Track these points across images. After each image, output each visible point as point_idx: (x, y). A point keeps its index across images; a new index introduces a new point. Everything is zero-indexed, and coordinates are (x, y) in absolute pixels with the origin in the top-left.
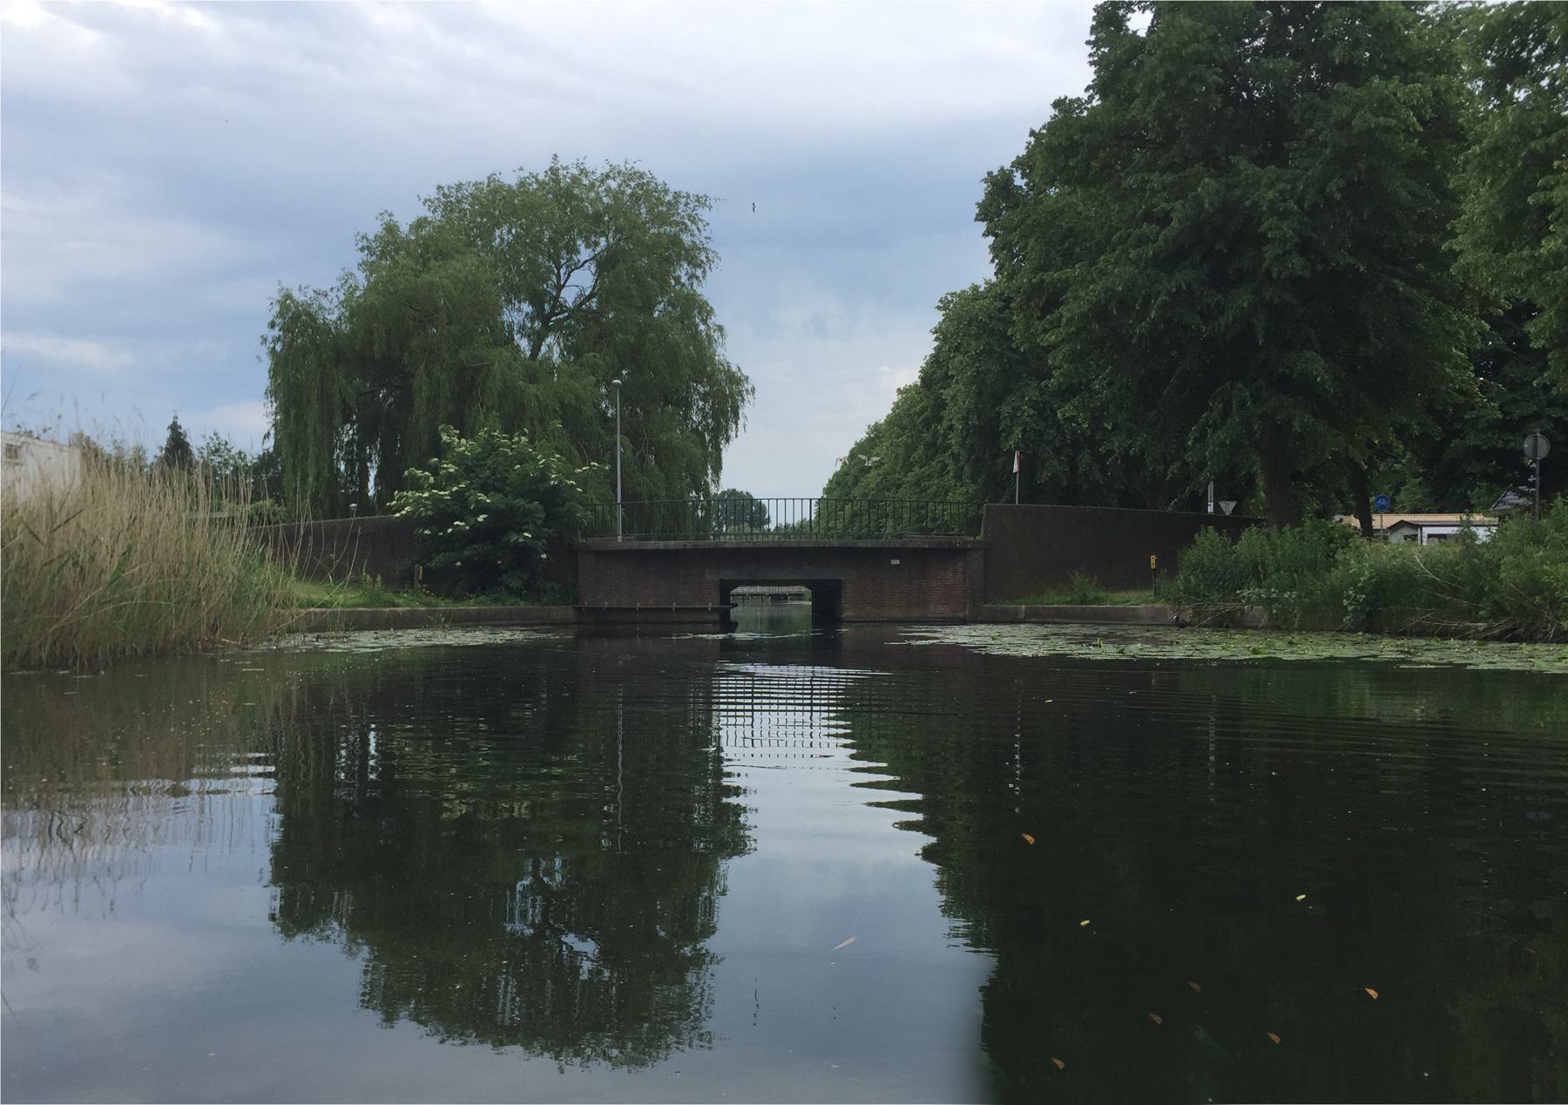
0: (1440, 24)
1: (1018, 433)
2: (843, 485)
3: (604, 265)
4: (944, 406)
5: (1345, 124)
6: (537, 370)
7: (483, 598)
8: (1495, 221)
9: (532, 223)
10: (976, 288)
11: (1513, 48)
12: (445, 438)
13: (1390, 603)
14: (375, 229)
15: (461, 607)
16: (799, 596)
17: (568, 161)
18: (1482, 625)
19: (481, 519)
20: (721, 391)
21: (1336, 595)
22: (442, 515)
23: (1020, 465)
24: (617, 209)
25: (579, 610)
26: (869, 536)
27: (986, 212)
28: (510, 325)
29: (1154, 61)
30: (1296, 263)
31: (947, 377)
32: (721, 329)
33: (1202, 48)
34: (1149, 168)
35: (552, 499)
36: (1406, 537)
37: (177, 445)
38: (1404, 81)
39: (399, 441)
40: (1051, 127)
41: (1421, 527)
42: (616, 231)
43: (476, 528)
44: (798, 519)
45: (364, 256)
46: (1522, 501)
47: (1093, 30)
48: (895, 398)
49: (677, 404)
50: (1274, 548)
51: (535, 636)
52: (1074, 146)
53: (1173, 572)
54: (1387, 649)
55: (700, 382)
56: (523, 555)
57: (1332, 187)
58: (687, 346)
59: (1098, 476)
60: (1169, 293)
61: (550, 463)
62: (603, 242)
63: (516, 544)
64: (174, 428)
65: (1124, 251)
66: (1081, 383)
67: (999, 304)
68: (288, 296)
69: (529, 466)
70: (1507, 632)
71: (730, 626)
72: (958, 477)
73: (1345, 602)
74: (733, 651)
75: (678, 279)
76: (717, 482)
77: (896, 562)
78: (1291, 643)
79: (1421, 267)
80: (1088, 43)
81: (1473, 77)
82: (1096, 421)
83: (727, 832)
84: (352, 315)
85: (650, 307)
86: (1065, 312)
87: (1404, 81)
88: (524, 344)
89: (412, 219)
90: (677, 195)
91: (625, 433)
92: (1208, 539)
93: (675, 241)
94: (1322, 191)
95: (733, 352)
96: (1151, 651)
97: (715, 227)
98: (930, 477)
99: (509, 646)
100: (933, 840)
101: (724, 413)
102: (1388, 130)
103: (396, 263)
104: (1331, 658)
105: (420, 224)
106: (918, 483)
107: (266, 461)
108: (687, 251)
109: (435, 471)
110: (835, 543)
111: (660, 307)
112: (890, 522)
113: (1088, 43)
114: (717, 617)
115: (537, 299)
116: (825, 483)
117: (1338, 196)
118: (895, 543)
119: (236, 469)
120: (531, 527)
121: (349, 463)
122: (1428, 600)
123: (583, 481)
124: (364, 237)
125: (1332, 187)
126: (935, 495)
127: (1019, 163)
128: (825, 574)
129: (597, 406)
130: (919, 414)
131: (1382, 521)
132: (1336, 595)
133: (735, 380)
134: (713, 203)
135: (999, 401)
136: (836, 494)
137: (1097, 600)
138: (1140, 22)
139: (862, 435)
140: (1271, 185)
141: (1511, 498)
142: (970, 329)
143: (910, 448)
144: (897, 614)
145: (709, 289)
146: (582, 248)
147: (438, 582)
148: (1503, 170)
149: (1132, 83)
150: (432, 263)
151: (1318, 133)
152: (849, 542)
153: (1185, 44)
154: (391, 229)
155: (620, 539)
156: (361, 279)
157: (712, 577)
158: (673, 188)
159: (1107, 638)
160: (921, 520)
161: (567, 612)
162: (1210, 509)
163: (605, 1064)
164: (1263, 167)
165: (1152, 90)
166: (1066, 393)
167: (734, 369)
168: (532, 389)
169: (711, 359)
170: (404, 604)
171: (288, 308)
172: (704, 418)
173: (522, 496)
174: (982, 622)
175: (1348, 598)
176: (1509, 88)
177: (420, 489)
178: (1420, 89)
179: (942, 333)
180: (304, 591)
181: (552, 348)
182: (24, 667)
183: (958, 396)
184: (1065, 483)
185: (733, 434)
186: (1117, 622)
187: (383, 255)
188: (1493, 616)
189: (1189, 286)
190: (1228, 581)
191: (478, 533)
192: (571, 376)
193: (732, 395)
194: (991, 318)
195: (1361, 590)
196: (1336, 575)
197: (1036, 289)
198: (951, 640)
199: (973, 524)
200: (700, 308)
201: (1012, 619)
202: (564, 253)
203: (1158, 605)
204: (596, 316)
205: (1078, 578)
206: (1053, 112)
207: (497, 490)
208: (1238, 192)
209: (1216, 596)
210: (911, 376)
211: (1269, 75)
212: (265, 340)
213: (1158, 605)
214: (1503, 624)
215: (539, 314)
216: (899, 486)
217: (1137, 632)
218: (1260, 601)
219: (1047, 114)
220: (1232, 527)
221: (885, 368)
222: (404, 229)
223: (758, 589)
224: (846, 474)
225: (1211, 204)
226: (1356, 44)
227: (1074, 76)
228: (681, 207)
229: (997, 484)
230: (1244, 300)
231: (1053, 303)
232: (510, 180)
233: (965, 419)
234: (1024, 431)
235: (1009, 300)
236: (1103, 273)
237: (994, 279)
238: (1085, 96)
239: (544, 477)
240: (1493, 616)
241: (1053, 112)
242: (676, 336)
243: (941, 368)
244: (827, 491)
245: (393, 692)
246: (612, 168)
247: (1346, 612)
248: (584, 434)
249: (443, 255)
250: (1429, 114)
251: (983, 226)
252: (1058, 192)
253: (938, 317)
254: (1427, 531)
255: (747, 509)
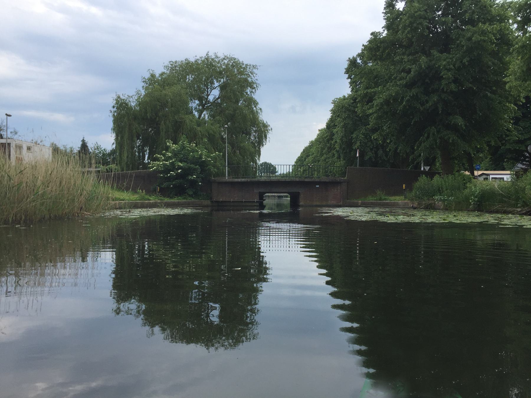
0: (502, 6)
1: (358, 144)
2: (300, 161)
3: (223, 88)
4: (333, 135)
5: (470, 39)
6: (200, 123)
7: (180, 198)
8: (523, 71)
9: (199, 74)
10: (344, 96)
11: (527, 13)
12: (168, 144)
13: (486, 201)
14: (147, 76)
15: (172, 201)
16: (287, 197)
17: (212, 55)
18: (519, 209)
19: (179, 171)
20: (261, 130)
21: (467, 199)
22: (167, 170)
23: (359, 154)
24: (227, 70)
25: (212, 202)
26: (308, 177)
27: (348, 71)
28: (192, 107)
29: (406, 18)
30: (453, 87)
31: (335, 126)
32: (261, 109)
33: (422, 13)
34: (404, 54)
35: (203, 165)
36: (484, 179)
37: (84, 146)
38: (490, 24)
39: (155, 145)
40: (370, 42)
41: (489, 175)
42: (227, 77)
43: (177, 174)
44: (285, 173)
45: (143, 84)
46: (524, 167)
47: (385, 8)
48: (318, 132)
49: (247, 134)
50: (445, 181)
51: (195, 211)
52: (377, 48)
53: (411, 190)
54: (490, 218)
55: (254, 127)
56: (193, 183)
57: (465, 61)
58: (249, 115)
59: (385, 158)
60: (410, 96)
61: (202, 153)
62: (222, 80)
63: (191, 179)
64: (83, 141)
65: (395, 82)
66: (379, 127)
67: (352, 101)
68: (119, 97)
69: (195, 154)
70: (529, 212)
71: (262, 207)
72: (339, 157)
73: (471, 201)
74: (264, 218)
75: (247, 93)
76: (259, 159)
77: (318, 186)
78: (454, 216)
79: (494, 88)
80: (383, 13)
81: (513, 24)
82: (384, 141)
83: (261, 271)
84: (139, 104)
85: (237, 102)
86: (375, 103)
87: (490, 24)
88: (196, 114)
89: (160, 72)
90: (247, 65)
91: (229, 143)
92: (423, 180)
93: (246, 80)
94: (461, 62)
95: (265, 117)
96: (406, 219)
97: (258, 77)
98: (329, 158)
99: (185, 215)
100: (336, 289)
101: (262, 137)
102: (484, 41)
103: (154, 87)
104: (471, 222)
105: (162, 74)
106: (325, 160)
107: (113, 152)
108: (250, 83)
109: (164, 155)
110: (297, 179)
111: (241, 102)
112: (316, 173)
113: (383, 13)
114: (258, 204)
115: (200, 99)
116: (295, 160)
117: (467, 63)
118: (317, 180)
119: (104, 155)
120: (196, 174)
121: (139, 153)
122: (495, 201)
123: (215, 158)
124: (144, 78)
125: (465, 61)
126: (331, 164)
127: (359, 55)
128: (295, 190)
129: (220, 134)
130: (326, 138)
131: (476, 173)
132: (467, 199)
133: (265, 126)
134: (259, 67)
135: (352, 133)
136: (299, 163)
137: (385, 199)
138: (400, 6)
139: (307, 144)
140: (445, 60)
141: (520, 165)
142: (343, 110)
143: (323, 149)
144: (318, 203)
145: (257, 96)
146: (215, 82)
147: (164, 192)
148: (526, 53)
149: (398, 26)
150: (166, 87)
151: (461, 42)
152: (302, 179)
153: (416, 12)
154: (153, 76)
155: (227, 178)
156: (143, 92)
157: (256, 191)
158: (245, 63)
159: (391, 213)
160: (326, 172)
161: (208, 202)
162: (422, 169)
163: (223, 348)
164: (442, 53)
165: (405, 28)
166: (374, 130)
167: (265, 122)
168: (199, 129)
169: (258, 119)
170: (153, 199)
171: (119, 101)
172: (255, 138)
173: (193, 163)
174: (346, 206)
175: (471, 199)
176: (526, 27)
177: (159, 161)
178: (496, 26)
179: (333, 111)
180: (118, 194)
181: (206, 115)
182: (5, 224)
183: (339, 132)
184: (374, 160)
185: (264, 143)
186: (392, 207)
187: (150, 85)
188: (523, 206)
189: (417, 94)
190: (430, 193)
191: (178, 176)
192: (212, 124)
193: (264, 131)
194: (349, 106)
195: (476, 197)
196: (467, 191)
197: (366, 95)
198: (336, 214)
199: (343, 174)
200: (254, 102)
201: (356, 206)
202: (209, 84)
203: (406, 201)
204: (220, 105)
205: (378, 192)
206: (370, 36)
207: (185, 161)
208: (433, 62)
209: (426, 198)
210: (323, 125)
211: (444, 23)
212: (111, 112)
213: (406, 201)
214: (526, 209)
215: (201, 104)
216: (319, 161)
217: (400, 211)
218: (441, 200)
219: (369, 37)
220: (431, 174)
221: (315, 123)
222: (157, 75)
223: (274, 194)
224: (302, 157)
225: (425, 66)
226: (473, 12)
227: (378, 25)
228: (248, 69)
229: (351, 161)
230: (435, 98)
231: (370, 100)
232: (192, 60)
233: (341, 140)
234: (360, 143)
235: (356, 99)
236: (388, 89)
237: (350, 93)
238: (381, 31)
239: (201, 157)
240: (523, 206)
241: (370, 36)
242: (246, 111)
243: (333, 122)
244: (296, 162)
245: (150, 229)
246: (225, 56)
247: (470, 204)
248: (214, 142)
249: (168, 84)
250: (498, 36)
251: (347, 76)
252: (373, 63)
253: (332, 106)
254: (491, 176)
255: (269, 168)
